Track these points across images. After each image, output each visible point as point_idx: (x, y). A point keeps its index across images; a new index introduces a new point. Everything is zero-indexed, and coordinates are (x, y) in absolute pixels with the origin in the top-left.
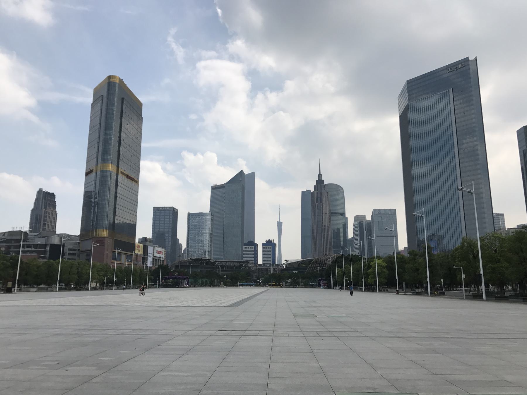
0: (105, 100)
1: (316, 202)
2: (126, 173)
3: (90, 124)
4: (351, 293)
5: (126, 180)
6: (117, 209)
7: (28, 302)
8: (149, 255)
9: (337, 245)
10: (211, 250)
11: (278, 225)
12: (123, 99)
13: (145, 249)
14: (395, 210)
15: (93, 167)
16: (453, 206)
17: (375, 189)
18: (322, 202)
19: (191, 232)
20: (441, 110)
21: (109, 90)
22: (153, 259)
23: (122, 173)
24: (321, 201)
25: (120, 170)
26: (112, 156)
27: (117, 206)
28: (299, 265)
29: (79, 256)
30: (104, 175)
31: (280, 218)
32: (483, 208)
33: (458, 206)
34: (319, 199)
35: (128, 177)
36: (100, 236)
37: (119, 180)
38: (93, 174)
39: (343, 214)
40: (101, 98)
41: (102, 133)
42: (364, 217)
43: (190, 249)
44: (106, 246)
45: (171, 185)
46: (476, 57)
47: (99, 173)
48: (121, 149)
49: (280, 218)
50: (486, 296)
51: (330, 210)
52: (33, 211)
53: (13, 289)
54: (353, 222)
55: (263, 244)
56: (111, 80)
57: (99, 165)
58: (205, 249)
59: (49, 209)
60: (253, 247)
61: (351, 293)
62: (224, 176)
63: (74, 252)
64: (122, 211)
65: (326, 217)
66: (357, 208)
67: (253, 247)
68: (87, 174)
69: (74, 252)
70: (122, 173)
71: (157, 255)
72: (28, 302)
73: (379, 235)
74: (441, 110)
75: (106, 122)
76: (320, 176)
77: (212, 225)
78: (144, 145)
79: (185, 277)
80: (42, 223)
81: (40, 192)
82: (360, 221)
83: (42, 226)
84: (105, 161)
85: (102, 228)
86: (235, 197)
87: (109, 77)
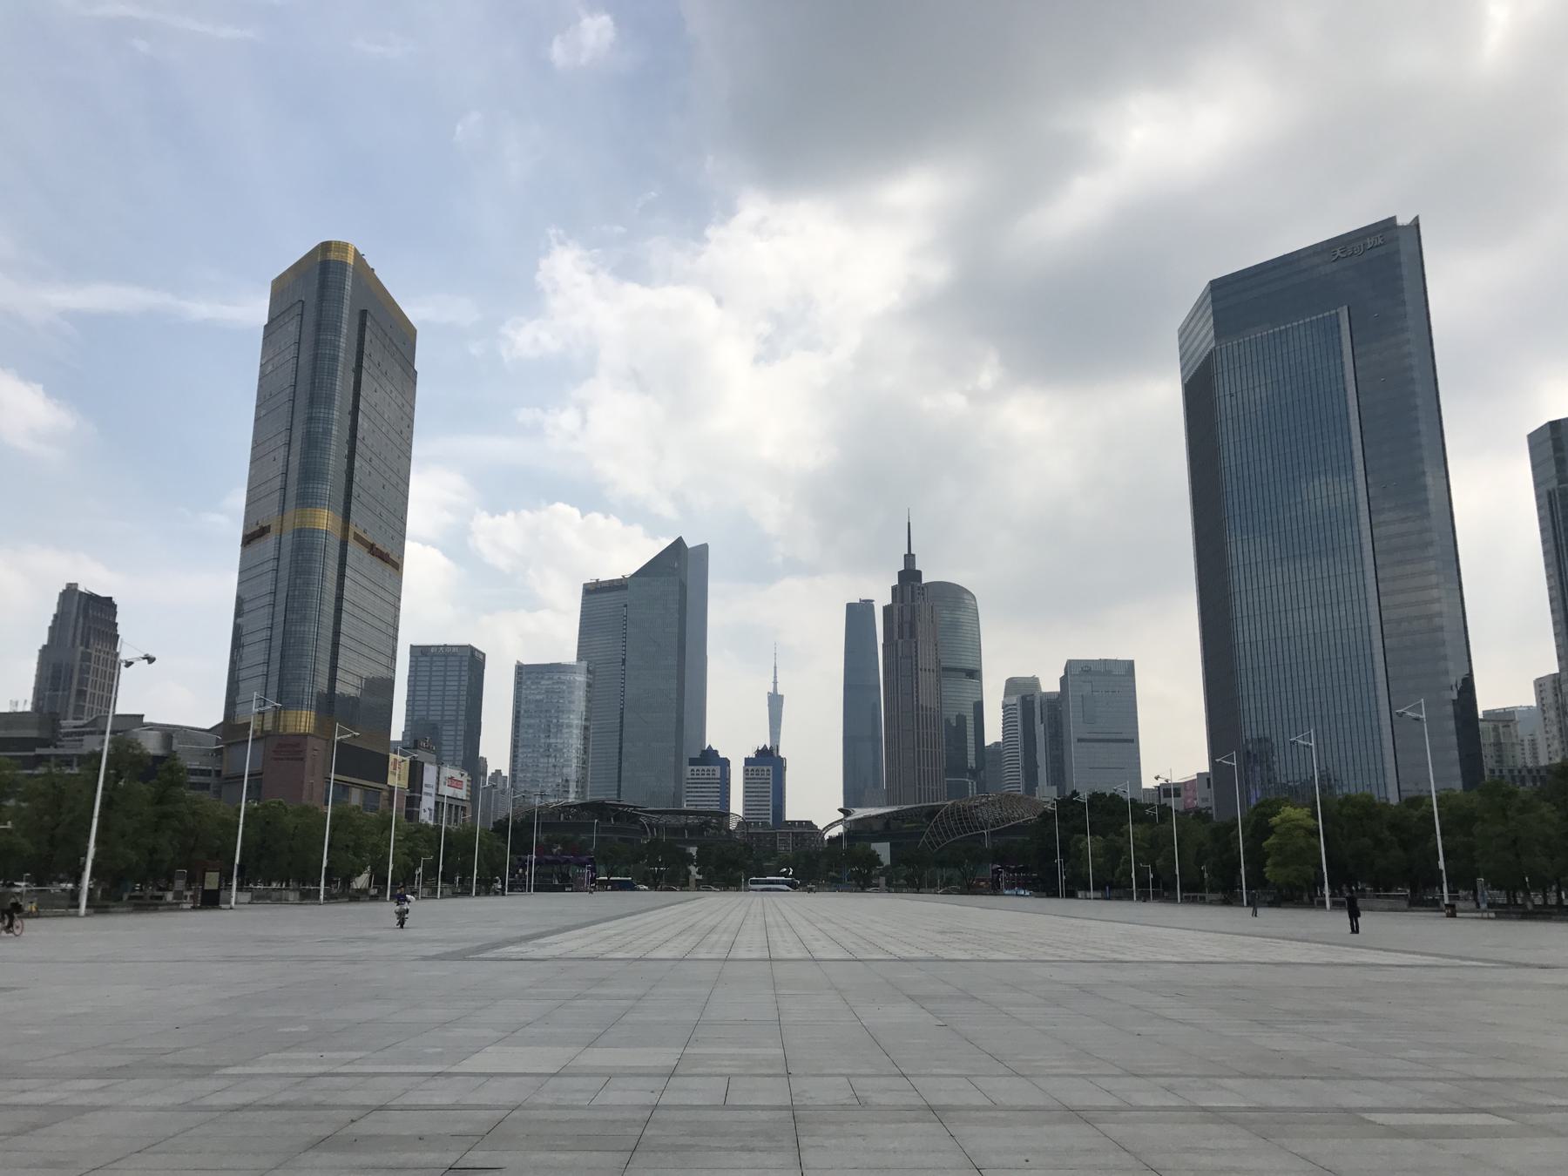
0: (310, 316)
1: (896, 636)
2: (369, 538)
3: (260, 386)
4: (1255, 914)
5: (368, 557)
6: (341, 650)
7: (1293, 952)
8: (425, 789)
9: (957, 766)
10: (584, 777)
11: (777, 700)
12: (364, 313)
13: (416, 772)
14: (1131, 664)
15: (269, 515)
16: (1354, 653)
17: (1103, 599)
18: (912, 640)
19: (523, 721)
20: (1309, 374)
21: (323, 286)
22: (437, 803)
23: (357, 538)
24: (913, 634)
25: (352, 527)
26: (331, 487)
27: (343, 639)
28: (887, 825)
29: (218, 793)
30: (304, 542)
31: (775, 683)
32: (1445, 658)
33: (1368, 652)
34: (906, 626)
35: (372, 549)
36: (290, 730)
37: (349, 560)
38: (270, 542)
39: (974, 674)
40: (297, 310)
41: (301, 416)
42: (1034, 682)
43: (521, 775)
44: (308, 763)
45: (486, 575)
46: (1417, 218)
47: (288, 538)
48: (357, 464)
49: (775, 683)
50: (87, 907)
51: (938, 662)
52: (44, 651)
53: (223, 894)
54: (1001, 698)
55: (748, 761)
56: (333, 256)
57: (289, 515)
58: (569, 777)
59: (96, 648)
60: (718, 769)
61: (1255, 914)
62: (625, 557)
63: (202, 779)
64: (355, 656)
65: (926, 681)
66: (1017, 654)
67: (718, 769)
68: (248, 540)
69: (202, 779)
70: (357, 538)
71: (447, 791)
72: (1293, 952)
73: (1087, 736)
74: (1309, 374)
75: (313, 383)
76: (909, 558)
77: (589, 701)
78: (417, 451)
79: (584, 859)
80: (74, 692)
81: (70, 594)
82: (1022, 695)
83: (72, 700)
84: (307, 499)
85: (299, 704)
86: (651, 619)
87: (326, 246)
